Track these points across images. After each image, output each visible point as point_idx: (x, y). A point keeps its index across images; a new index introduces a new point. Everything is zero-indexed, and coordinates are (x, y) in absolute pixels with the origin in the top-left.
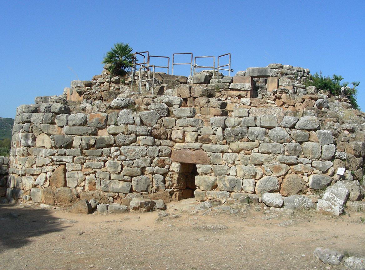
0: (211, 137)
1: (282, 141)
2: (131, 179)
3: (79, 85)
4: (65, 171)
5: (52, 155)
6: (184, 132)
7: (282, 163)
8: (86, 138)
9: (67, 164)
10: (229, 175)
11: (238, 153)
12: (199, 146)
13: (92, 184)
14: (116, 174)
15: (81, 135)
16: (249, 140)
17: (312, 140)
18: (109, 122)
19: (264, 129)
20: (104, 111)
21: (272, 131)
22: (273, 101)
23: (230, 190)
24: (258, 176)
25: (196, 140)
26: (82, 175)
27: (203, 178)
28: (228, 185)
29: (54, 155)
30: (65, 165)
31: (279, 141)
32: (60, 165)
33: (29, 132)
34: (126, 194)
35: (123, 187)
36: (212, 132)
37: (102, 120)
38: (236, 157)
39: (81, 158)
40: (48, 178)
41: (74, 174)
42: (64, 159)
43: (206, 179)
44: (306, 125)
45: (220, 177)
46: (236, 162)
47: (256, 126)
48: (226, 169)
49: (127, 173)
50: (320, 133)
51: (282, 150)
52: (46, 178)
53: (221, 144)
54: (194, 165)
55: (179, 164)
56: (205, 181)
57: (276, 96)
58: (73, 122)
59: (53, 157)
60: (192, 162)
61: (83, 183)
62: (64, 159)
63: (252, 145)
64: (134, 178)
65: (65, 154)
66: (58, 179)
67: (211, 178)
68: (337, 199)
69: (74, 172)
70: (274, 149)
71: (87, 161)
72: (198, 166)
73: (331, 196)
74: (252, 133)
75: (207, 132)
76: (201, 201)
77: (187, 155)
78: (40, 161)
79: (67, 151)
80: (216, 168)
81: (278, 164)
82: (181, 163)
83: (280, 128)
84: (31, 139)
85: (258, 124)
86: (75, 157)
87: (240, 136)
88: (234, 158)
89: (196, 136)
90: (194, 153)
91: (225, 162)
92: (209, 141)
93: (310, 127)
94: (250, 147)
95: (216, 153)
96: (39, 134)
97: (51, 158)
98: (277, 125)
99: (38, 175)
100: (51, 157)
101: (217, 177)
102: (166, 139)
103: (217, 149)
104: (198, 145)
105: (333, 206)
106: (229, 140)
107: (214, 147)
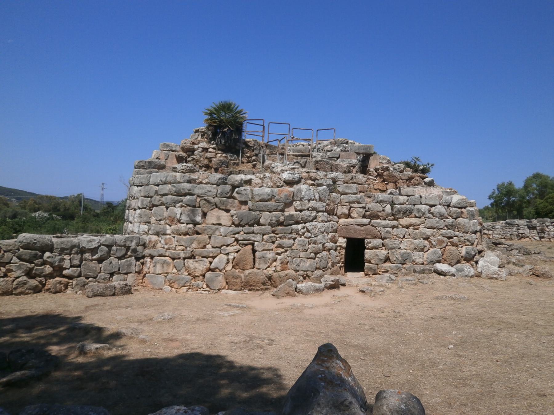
0: (380, 214)
1: (442, 217)
2: (316, 256)
3: (174, 149)
4: (254, 251)
5: (235, 234)
6: (351, 207)
7: (444, 237)
8: (276, 214)
9: (256, 243)
10: (400, 248)
11: (407, 228)
12: (368, 222)
13: (284, 264)
14: (305, 252)
15: (270, 212)
16: (416, 217)
17: (463, 216)
18: (295, 198)
19: (428, 207)
20: (281, 185)
21: (435, 208)
22: (375, 177)
23: (403, 262)
24: (426, 249)
25: (364, 217)
26: (274, 254)
27: (375, 252)
28: (400, 259)
29: (238, 233)
30: (253, 245)
31: (440, 218)
32: (246, 245)
33: (194, 206)
34: (313, 272)
35: (310, 265)
36: (381, 209)
37: (290, 195)
38: (406, 232)
39: (273, 237)
40: (231, 260)
41: (266, 254)
42: (252, 237)
43: (378, 253)
44: (459, 203)
45: (392, 250)
46: (406, 237)
47: (421, 204)
48: (398, 243)
49: (314, 251)
50: (468, 211)
51: (444, 225)
52: (228, 260)
53: (389, 220)
54: (363, 240)
55: (345, 240)
56: (377, 255)
57: (378, 173)
58: (260, 197)
59: (237, 236)
60: (361, 237)
61: (274, 264)
62: (252, 237)
63: (420, 221)
64: (318, 255)
65: (253, 233)
66: (246, 260)
67: (383, 253)
68: (492, 266)
69: (265, 252)
70: (438, 225)
71: (279, 239)
72: (366, 241)
73: (485, 264)
74: (419, 210)
75: (377, 209)
76: (372, 274)
77: (355, 231)
78: (217, 240)
79: (256, 228)
80: (387, 242)
81: (441, 238)
82: (347, 238)
83: (440, 206)
84: (200, 215)
85: (423, 201)
86: (265, 235)
87: (407, 213)
88: (404, 233)
89: (364, 212)
90: (362, 228)
91: (395, 237)
92: (378, 217)
93: (462, 205)
94: (419, 223)
95: (387, 229)
96: (212, 210)
97: (233, 237)
98: (438, 204)
99: (214, 257)
100: (234, 236)
101: (389, 251)
102: (333, 215)
103: (387, 225)
104: (366, 221)
105: (499, 272)
106: (397, 216)
107: (384, 223)
